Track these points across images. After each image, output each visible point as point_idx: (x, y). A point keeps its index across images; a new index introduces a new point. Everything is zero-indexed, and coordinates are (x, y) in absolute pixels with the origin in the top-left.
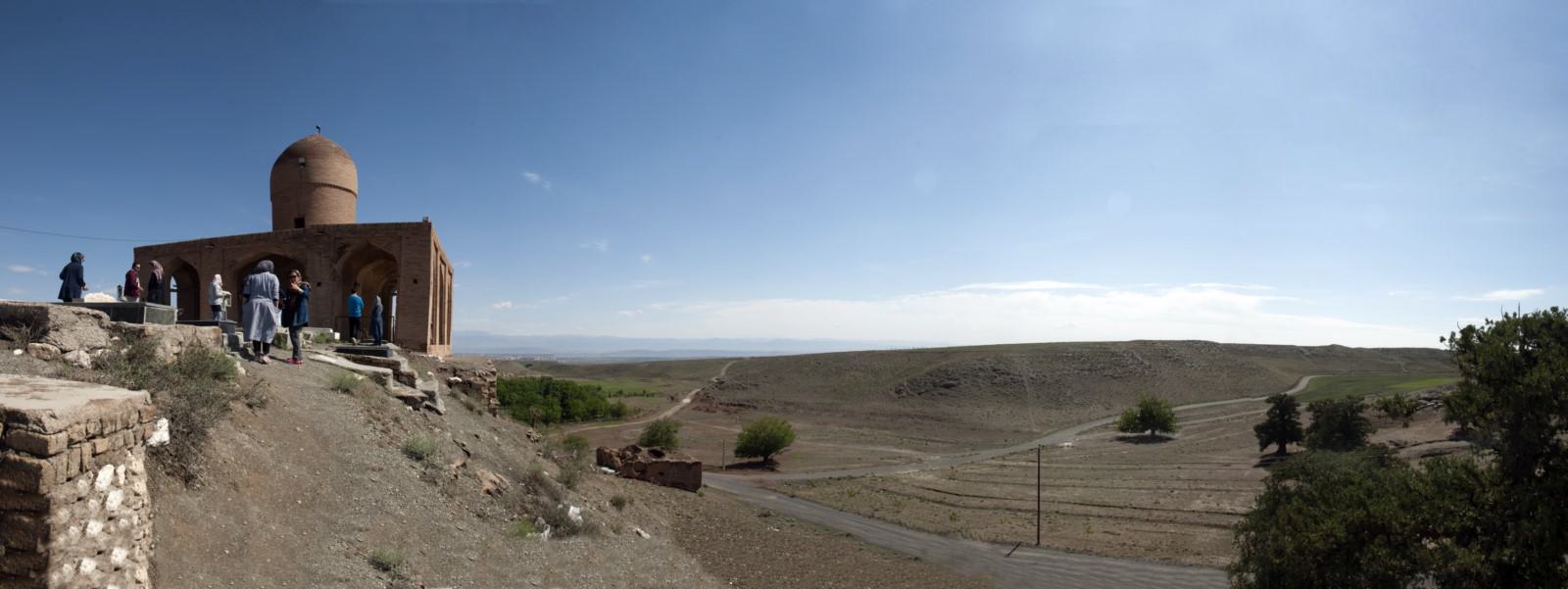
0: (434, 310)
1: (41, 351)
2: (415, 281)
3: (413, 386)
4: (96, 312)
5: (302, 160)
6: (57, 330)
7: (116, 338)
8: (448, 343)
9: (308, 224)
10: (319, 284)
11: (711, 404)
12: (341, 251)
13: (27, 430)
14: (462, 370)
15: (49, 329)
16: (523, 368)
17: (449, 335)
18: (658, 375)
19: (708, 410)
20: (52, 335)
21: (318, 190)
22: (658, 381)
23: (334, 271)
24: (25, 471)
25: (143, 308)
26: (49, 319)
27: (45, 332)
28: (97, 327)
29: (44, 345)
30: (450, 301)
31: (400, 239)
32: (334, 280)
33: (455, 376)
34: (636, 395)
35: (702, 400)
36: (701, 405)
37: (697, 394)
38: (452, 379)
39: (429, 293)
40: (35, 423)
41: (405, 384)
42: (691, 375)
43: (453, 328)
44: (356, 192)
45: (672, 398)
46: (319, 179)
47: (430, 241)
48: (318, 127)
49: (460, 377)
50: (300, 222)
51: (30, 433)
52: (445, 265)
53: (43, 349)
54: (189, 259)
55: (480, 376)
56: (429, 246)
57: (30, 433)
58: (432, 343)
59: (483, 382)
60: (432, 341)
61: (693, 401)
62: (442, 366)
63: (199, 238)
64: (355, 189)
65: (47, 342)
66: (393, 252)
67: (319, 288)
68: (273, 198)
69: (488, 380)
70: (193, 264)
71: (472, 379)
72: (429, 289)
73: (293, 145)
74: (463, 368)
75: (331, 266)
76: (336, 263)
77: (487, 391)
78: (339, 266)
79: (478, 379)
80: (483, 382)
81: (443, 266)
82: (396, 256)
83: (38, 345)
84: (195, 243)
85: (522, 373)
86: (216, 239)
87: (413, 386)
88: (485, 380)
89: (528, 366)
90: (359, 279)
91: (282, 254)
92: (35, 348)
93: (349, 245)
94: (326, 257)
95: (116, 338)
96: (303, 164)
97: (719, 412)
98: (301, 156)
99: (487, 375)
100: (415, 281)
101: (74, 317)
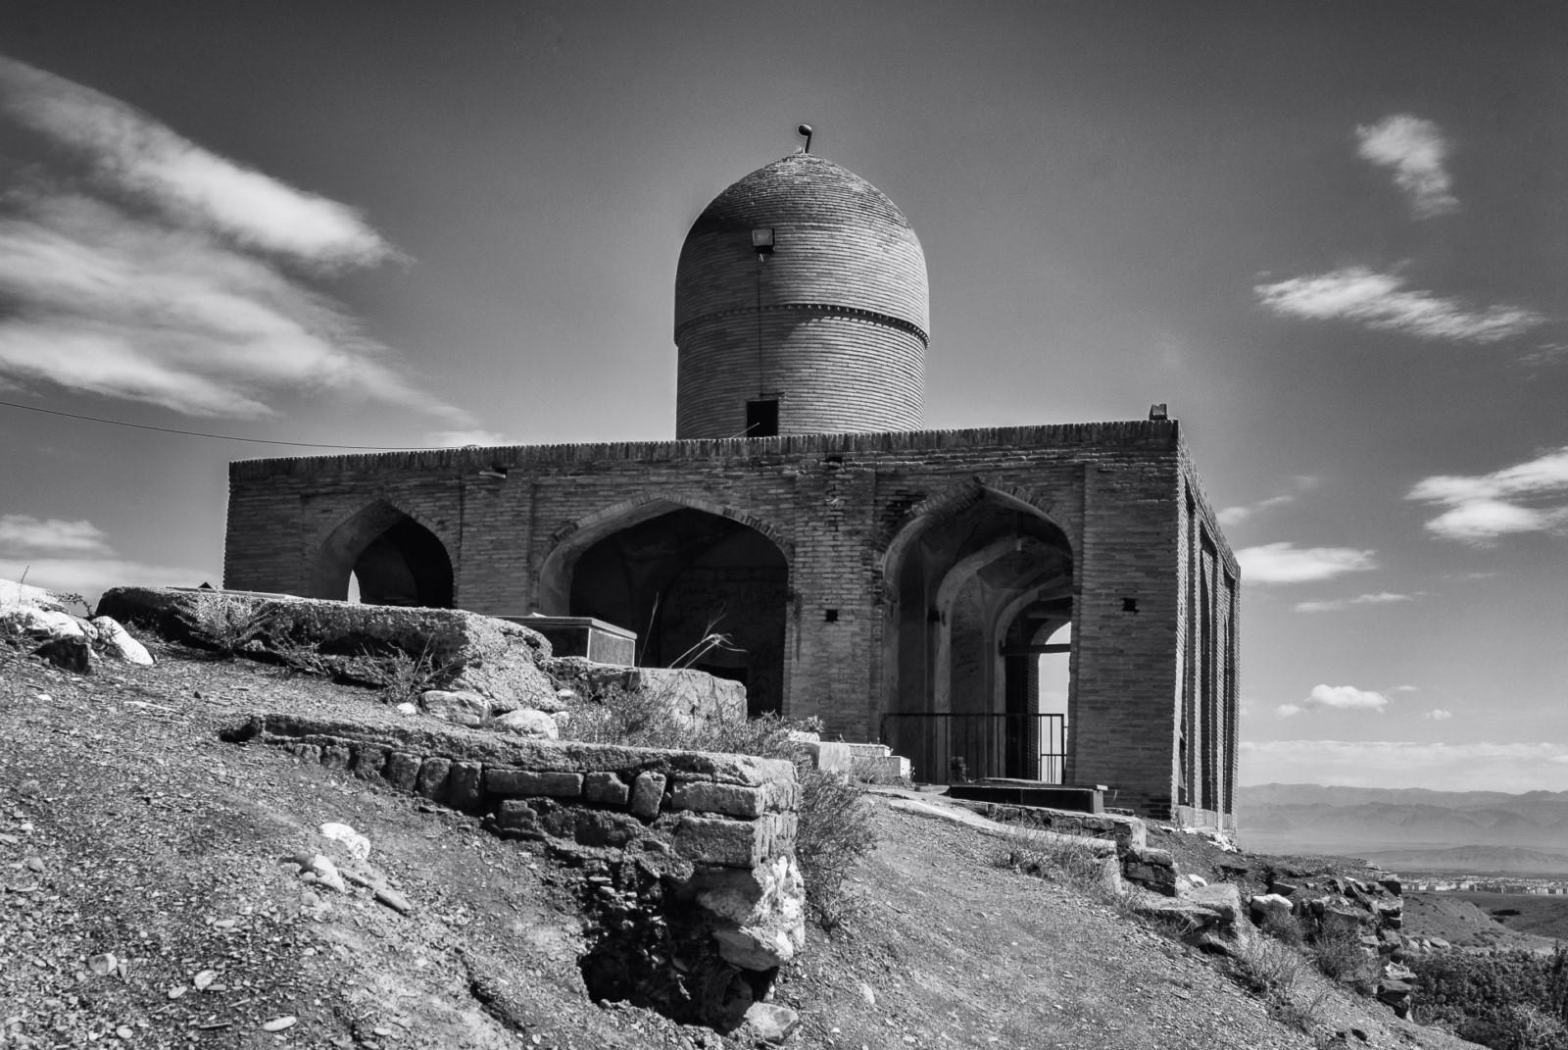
0: (1188, 695)
1: (457, 708)
3: (1169, 891)
4: (532, 633)
5: (761, 237)
6: (478, 666)
7: (568, 693)
8: (1228, 809)
9: (789, 428)
12: (896, 515)
13: (714, 781)
14: (1291, 875)
15: (464, 662)
16: (1482, 920)
17: (1228, 783)
20: (469, 673)
21: (812, 327)
23: (877, 575)
24: (724, 836)
25: (587, 631)
26: (466, 640)
27: (457, 670)
28: (532, 667)
29: (463, 695)
30: (1230, 671)
32: (878, 602)
33: (1269, 892)
38: (1263, 899)
39: (1173, 642)
40: (724, 771)
41: (1145, 884)
43: (1243, 744)
46: (813, 293)
47: (1172, 479)
48: (803, 131)
49: (1286, 892)
50: (763, 416)
51: (719, 785)
52: (1213, 553)
53: (462, 704)
55: (1349, 893)
56: (1172, 493)
57: (719, 785)
58: (1186, 800)
59: (1357, 912)
60: (1181, 791)
62: (1227, 861)
64: (921, 316)
65: (461, 687)
66: (1060, 515)
67: (831, 628)
69: (1377, 905)
71: (1325, 899)
72: (1173, 627)
74: (1295, 869)
75: (866, 560)
76: (882, 550)
77: (1374, 940)
78: (887, 561)
79: (1345, 901)
80: (1365, 913)
81: (1208, 558)
82: (1066, 527)
83: (447, 695)
85: (1481, 938)
87: (1169, 891)
88: (1367, 907)
89: (1501, 915)
90: (946, 598)
91: (718, 510)
92: (444, 702)
93: (920, 496)
94: (850, 533)
95: (568, 693)
96: (767, 250)
98: (756, 226)
99: (1371, 891)
101: (501, 640)
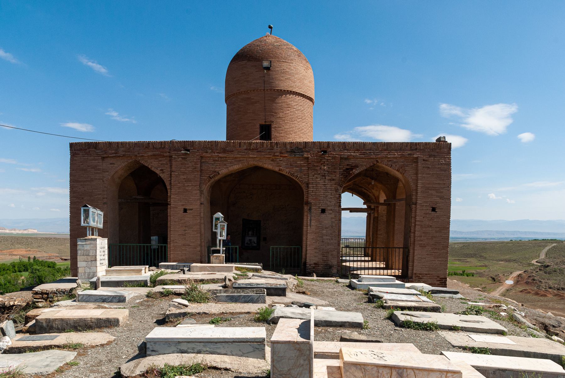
2: (434, 210)
5: (266, 64)
10: (323, 211)
11: (539, 287)
18: (472, 256)
19: (537, 294)
22: (474, 261)
31: (416, 160)
34: (455, 274)
35: (527, 283)
36: (527, 288)
37: (519, 276)
42: (507, 257)
44: (313, 97)
45: (494, 279)
46: (284, 85)
48: (270, 27)
54: (154, 165)
61: (517, 282)
63: (168, 139)
67: (323, 216)
68: (229, 99)
70: (158, 172)
73: (250, 45)
84: (162, 145)
86: (193, 143)
91: (277, 169)
96: (268, 69)
97: (550, 296)
100: (434, 210)
